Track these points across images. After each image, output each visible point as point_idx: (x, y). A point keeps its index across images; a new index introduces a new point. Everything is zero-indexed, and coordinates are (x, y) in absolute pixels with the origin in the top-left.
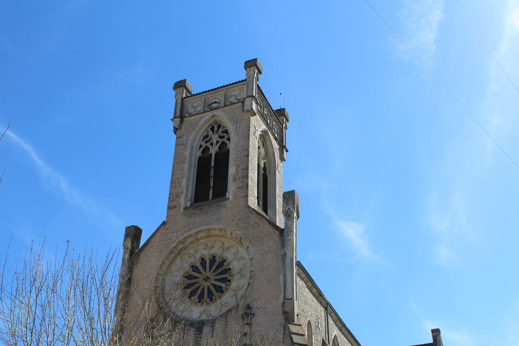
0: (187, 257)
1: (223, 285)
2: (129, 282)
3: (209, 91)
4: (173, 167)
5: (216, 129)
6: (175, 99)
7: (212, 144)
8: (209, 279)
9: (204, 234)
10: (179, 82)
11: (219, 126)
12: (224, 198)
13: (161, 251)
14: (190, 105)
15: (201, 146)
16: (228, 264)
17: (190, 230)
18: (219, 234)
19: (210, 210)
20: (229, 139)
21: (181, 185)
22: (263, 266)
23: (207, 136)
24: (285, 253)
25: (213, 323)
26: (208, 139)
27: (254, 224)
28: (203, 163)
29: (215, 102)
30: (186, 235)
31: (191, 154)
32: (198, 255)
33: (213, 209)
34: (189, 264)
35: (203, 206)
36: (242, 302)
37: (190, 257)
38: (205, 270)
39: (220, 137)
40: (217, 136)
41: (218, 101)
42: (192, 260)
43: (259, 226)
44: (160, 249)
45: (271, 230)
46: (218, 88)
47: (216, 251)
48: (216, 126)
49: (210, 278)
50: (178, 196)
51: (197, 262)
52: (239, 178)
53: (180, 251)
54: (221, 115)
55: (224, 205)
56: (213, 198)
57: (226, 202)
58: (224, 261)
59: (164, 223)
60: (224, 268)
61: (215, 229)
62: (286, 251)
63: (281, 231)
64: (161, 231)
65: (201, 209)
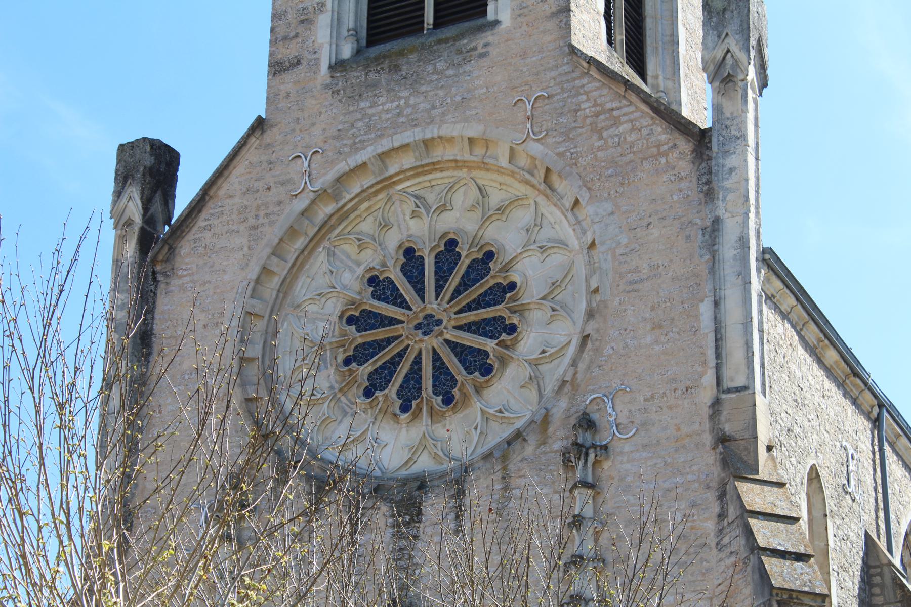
0: (350, 249)
1: (489, 345)
2: (145, 341)
8: (436, 321)
9: (408, 161)
12: (480, 21)
13: (254, 228)
17: (355, 148)
18: (467, 157)
19: (430, 68)
22: (637, 270)
24: (717, 221)
25: (457, 482)
27: (597, 115)
30: (342, 167)
32: (393, 240)
33: (440, 65)
34: (360, 271)
35: (401, 53)
36: (563, 403)
37: (361, 248)
42: (370, 258)
43: (616, 122)
44: (252, 221)
45: (663, 137)
47: (459, 220)
49: (439, 322)
51: (390, 263)
53: (326, 227)
55: (480, 50)
58: (490, 255)
59: (259, 125)
60: (489, 282)
61: (450, 140)
62: (721, 212)
63: (701, 139)
64: (251, 155)
65: (396, 68)
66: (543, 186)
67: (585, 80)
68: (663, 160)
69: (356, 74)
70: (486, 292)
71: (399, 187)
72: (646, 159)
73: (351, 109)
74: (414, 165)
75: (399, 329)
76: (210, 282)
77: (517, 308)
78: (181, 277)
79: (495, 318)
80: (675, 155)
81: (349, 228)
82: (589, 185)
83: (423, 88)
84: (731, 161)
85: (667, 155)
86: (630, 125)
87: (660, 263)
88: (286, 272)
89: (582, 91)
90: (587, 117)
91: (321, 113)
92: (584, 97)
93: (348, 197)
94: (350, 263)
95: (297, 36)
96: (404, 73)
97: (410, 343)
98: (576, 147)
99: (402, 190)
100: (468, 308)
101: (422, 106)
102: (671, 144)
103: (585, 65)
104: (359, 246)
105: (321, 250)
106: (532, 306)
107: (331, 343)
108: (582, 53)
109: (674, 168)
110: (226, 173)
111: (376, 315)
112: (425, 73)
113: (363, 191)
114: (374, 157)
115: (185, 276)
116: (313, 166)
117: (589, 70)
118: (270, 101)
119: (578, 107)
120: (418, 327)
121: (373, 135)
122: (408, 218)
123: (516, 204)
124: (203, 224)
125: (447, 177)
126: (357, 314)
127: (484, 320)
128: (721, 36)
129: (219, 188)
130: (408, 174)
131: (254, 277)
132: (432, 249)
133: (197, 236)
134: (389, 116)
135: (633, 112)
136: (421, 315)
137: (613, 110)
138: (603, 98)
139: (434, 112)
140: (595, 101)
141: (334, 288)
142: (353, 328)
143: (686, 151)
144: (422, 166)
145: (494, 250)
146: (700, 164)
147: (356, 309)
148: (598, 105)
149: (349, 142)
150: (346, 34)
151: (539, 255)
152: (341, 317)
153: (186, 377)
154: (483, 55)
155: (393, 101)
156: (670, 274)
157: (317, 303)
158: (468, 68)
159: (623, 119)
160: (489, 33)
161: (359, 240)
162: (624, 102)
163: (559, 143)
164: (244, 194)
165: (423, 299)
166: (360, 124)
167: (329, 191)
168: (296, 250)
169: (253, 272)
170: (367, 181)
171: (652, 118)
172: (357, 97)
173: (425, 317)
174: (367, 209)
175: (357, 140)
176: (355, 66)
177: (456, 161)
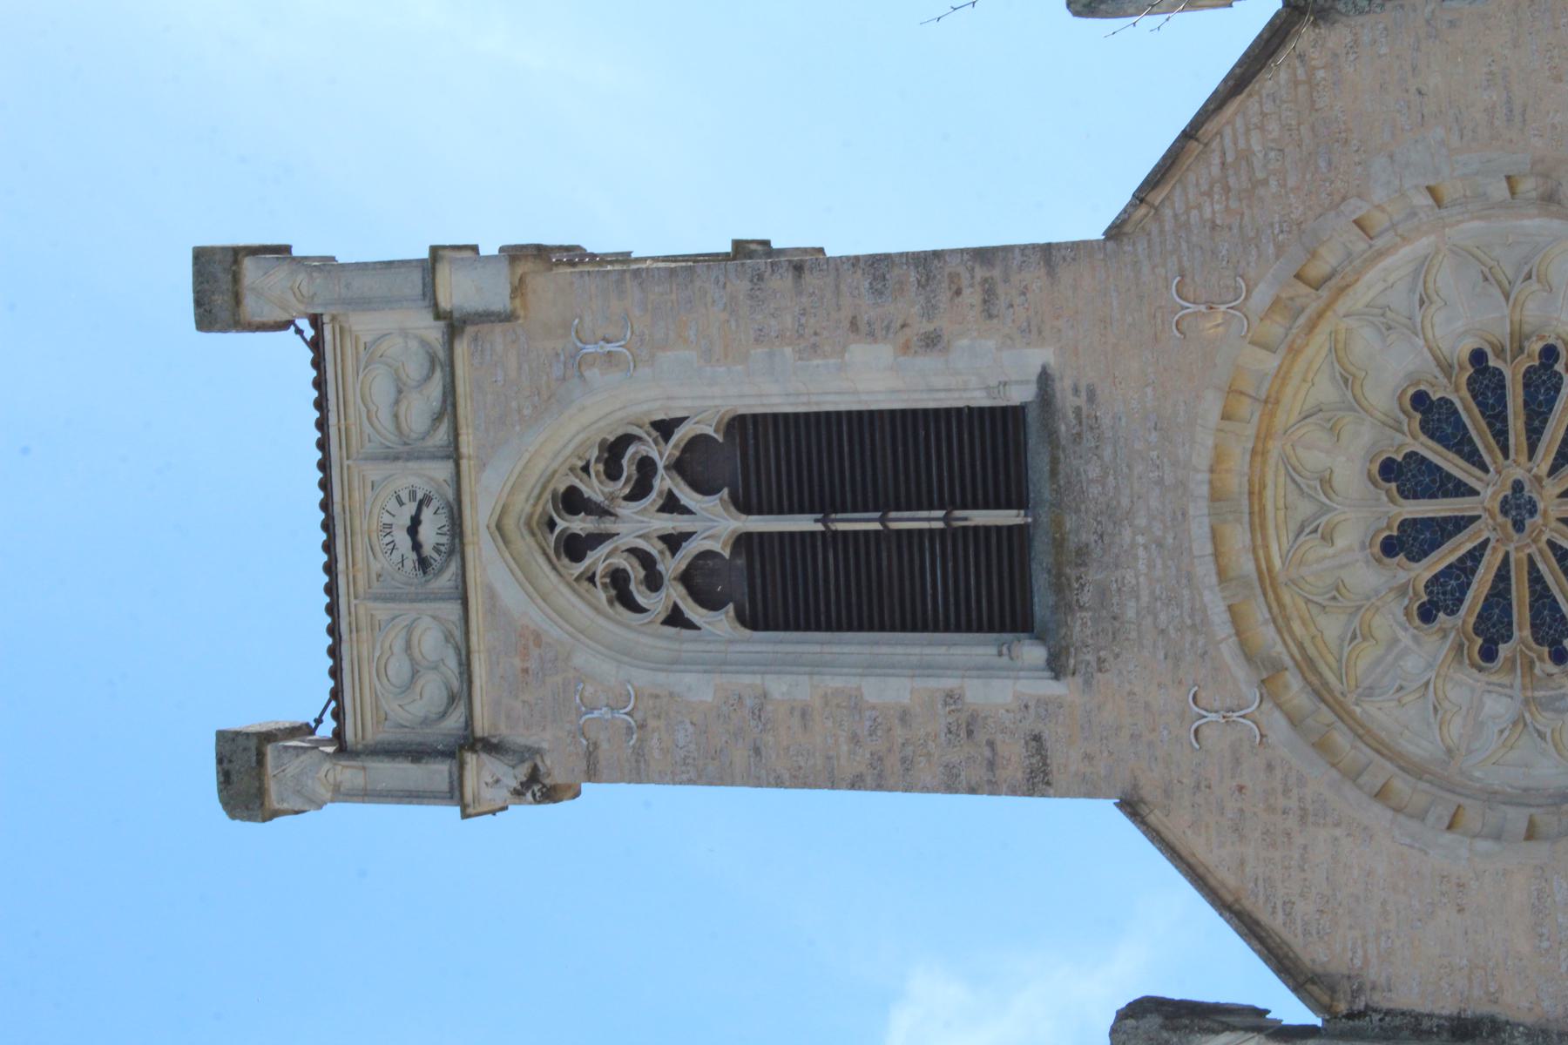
0: (1367, 655)
3: (330, 568)
4: (779, 783)
5: (580, 525)
6: (332, 809)
7: (673, 542)
9: (1238, 538)
10: (226, 779)
11: (572, 501)
12: (1032, 416)
13: (1303, 819)
14: (392, 706)
15: (676, 618)
16: (1446, 368)
18: (1251, 431)
19: (1095, 490)
20: (665, 428)
21: (905, 716)
23: (618, 580)
26: (636, 572)
27: (1227, 189)
28: (781, 593)
29: (413, 529)
30: (1228, 652)
31: (718, 666)
33: (1094, 471)
34: (1406, 639)
35: (1059, 544)
37: (1368, 636)
38: (1460, 524)
40: (627, 510)
41: (411, 508)
42: (1391, 621)
43: (1245, 156)
44: (1292, 823)
45: (1283, 76)
46: (326, 505)
47: (1348, 462)
48: (566, 526)
49: (1518, 486)
50: (970, 726)
51: (1403, 577)
52: (929, 311)
53: (1321, 693)
54: (507, 477)
55: (1082, 401)
56: (1021, 503)
57: (1067, 400)
58: (1420, 400)
59: (1132, 807)
60: (1461, 399)
64: (1176, 825)
65: (1082, 552)
66: (1325, 293)
67: (1168, 212)
68: (1321, 74)
69: (1078, 628)
70: (1479, 404)
71: (1277, 563)
72: (1313, 102)
73: (1133, 635)
74: (1247, 526)
75: (1543, 465)
76: (1384, 903)
77: (1516, 345)
78: (1366, 961)
79: (1526, 386)
80: (1315, 55)
81: (1331, 659)
82: (1337, 198)
83: (1125, 502)
85: (1315, 68)
86: (1253, 133)
87: (1485, 70)
88: (1388, 765)
89: (1183, 218)
90: (1227, 207)
91: (1131, 693)
92: (1194, 213)
93: (1279, 648)
94: (1390, 658)
95: (991, 744)
96: (1095, 537)
97: (1544, 538)
98: (1272, 225)
99: (1283, 558)
100: (1501, 436)
101: (1154, 503)
102: (1297, 63)
103: (1143, 210)
104: (1364, 639)
105: (1358, 710)
106: (1517, 318)
107: (1524, 688)
108: (1125, 211)
109: (1336, 55)
110: (1201, 870)
111: (1487, 605)
112: (1101, 499)
113: (1274, 621)
114: (1222, 590)
115: (1365, 952)
116: (1217, 705)
117: (1152, 206)
118: (1092, 793)
119: (1209, 224)
120: (1519, 526)
121: (1186, 592)
122: (1330, 551)
123: (1341, 354)
124: (1280, 916)
125: (1276, 476)
126: (1480, 641)
127: (1526, 404)
129: (1223, 885)
130: (1259, 542)
131: (1389, 814)
132: (1392, 500)
133: (1299, 931)
134: (1159, 562)
135: (1234, 130)
136: (1500, 519)
137: (1223, 164)
138: (1202, 181)
139: (1169, 479)
140: (1203, 194)
141: (1427, 684)
142: (1502, 647)
143: (1313, 36)
144: (1251, 513)
145: (1411, 392)
146: (1339, 12)
147: (1471, 641)
148: (1211, 188)
149: (1189, 637)
150: (1005, 659)
151: (1434, 307)
152: (1480, 670)
153: (1545, 944)
154: (1092, 396)
155: (1136, 558)
156: (1506, 52)
157: (1448, 717)
158: (1106, 422)
159: (1242, 144)
160: (1058, 385)
161: (1354, 637)
162: (1214, 145)
163: (1259, 256)
164: (1242, 838)
165: (1473, 519)
166: (1163, 617)
167: (1265, 676)
168: (1353, 747)
169: (1378, 815)
170: (1258, 613)
171: (1250, 95)
172: (1117, 624)
173: (1504, 512)
174: (1304, 623)
175: (1189, 622)
176: (1063, 631)
177: (1254, 452)
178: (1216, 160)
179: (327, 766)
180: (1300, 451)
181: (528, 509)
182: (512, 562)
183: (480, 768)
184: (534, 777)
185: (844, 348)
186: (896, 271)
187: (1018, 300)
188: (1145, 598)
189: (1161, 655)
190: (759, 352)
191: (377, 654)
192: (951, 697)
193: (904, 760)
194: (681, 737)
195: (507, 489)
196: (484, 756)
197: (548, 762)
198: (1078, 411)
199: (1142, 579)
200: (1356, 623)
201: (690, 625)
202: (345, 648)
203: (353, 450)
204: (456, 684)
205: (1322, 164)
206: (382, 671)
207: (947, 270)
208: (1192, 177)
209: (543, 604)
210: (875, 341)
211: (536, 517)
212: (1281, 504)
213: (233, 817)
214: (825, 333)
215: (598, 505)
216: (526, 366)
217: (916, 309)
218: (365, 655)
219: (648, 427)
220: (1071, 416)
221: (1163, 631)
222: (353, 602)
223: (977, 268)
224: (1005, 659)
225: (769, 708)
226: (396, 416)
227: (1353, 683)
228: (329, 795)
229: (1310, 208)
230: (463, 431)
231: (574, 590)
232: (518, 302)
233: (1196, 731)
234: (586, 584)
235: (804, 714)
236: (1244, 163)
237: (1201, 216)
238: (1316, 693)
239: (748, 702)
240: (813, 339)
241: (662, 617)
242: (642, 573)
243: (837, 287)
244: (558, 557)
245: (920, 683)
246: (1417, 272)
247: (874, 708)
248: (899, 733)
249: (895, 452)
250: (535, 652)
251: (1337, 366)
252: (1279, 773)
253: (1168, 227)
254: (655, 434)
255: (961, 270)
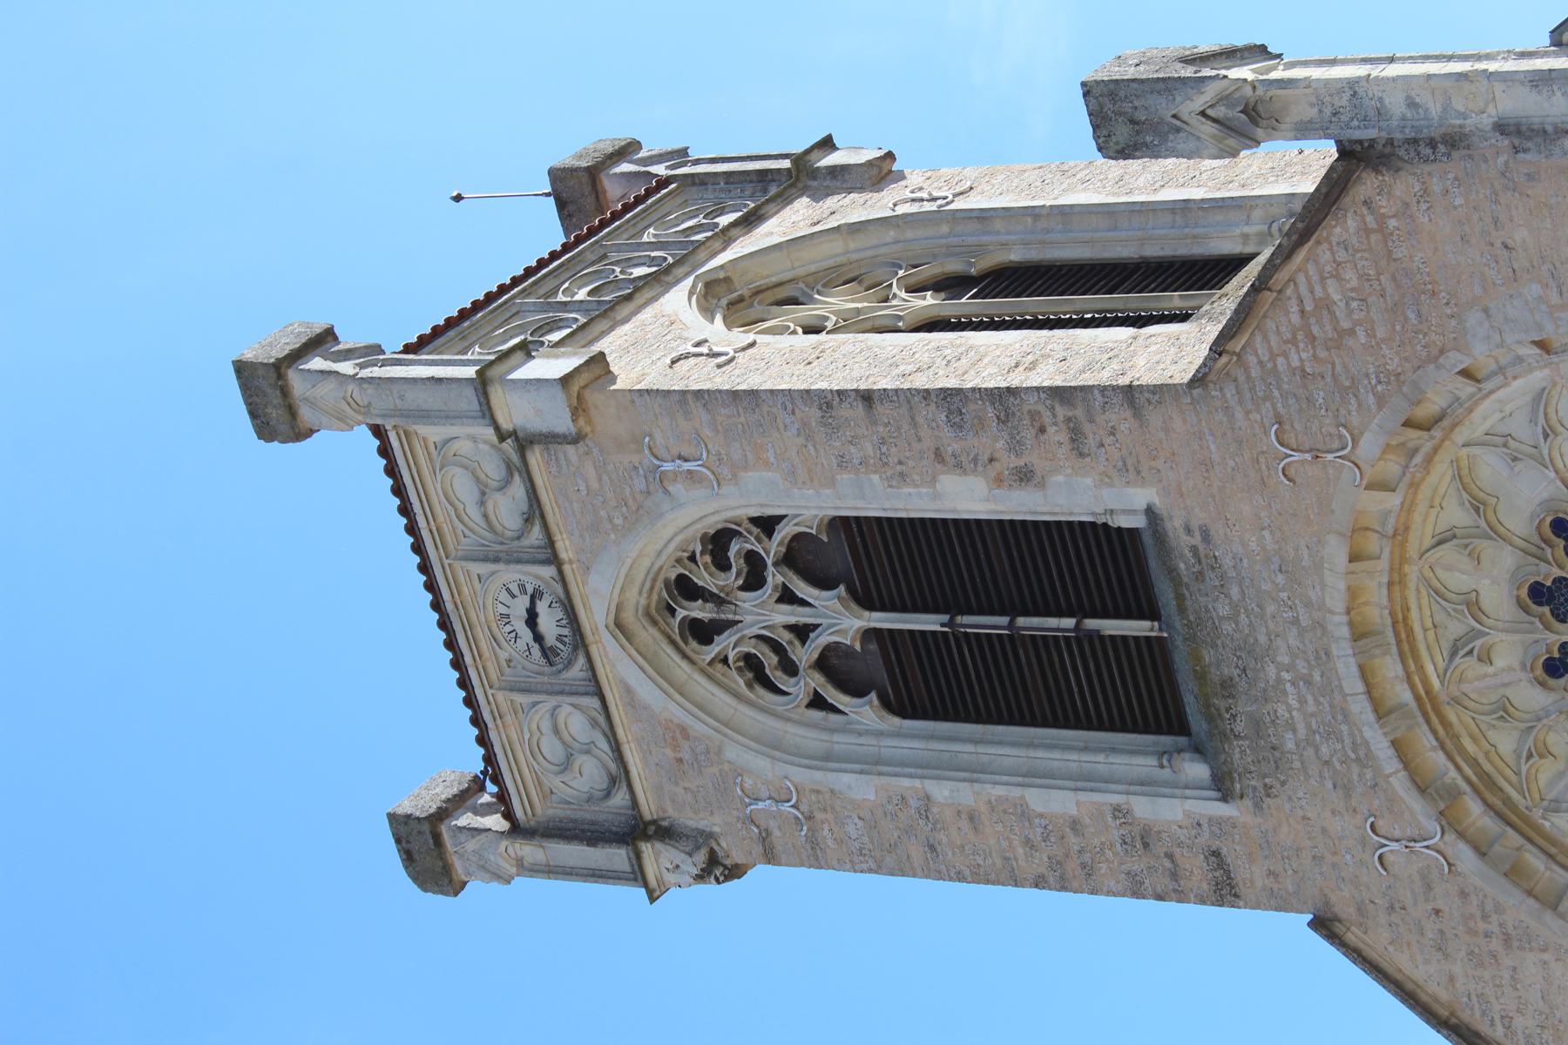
3: (457, 664)
5: (700, 611)
7: (802, 632)
9: (1389, 668)
10: (408, 858)
11: (686, 588)
12: (1147, 540)
13: (1507, 940)
15: (818, 702)
17: (1365, 759)
18: (1383, 564)
19: (1228, 627)
20: (767, 525)
21: (1075, 825)
23: (751, 663)
24: (1501, 128)
26: (770, 660)
28: (922, 685)
29: (532, 619)
30: (1399, 783)
31: (872, 764)
33: (1223, 610)
35: (1201, 677)
37: (1545, 752)
39: (754, 581)
40: (747, 600)
41: (524, 602)
43: (1325, 305)
44: (1496, 944)
45: (1351, 223)
46: (437, 605)
47: (1495, 582)
48: (687, 608)
50: (1145, 839)
52: (1015, 446)
53: (1507, 814)
54: (613, 577)
55: (1197, 540)
56: (1152, 614)
59: (1324, 925)
61: (1353, 593)
62: (1486, 121)
63: (1355, 157)
64: (1377, 942)
65: (1227, 686)
66: (1437, 433)
67: (1251, 359)
69: (1237, 756)
72: (1390, 252)
73: (1297, 765)
80: (1384, 203)
81: (1508, 772)
82: (1435, 352)
83: (1262, 639)
84: (1396, 104)
85: (1384, 216)
86: (1329, 282)
89: (1270, 365)
92: (1280, 360)
93: (1453, 773)
95: (1170, 856)
101: (1293, 642)
102: (1365, 210)
103: (1224, 359)
104: (1541, 756)
105: (1547, 824)
108: (1204, 364)
110: (1410, 986)
112: (1236, 636)
113: (1443, 747)
116: (1397, 834)
118: (1283, 906)
121: (1344, 728)
122: (1491, 670)
123: (1467, 480)
128: (1177, 126)
129: (1437, 1000)
130: (1412, 667)
132: (1548, 627)
134: (1310, 699)
138: (1283, 329)
144: (1399, 643)
145: (1549, 519)
146: (1400, 158)
148: (1294, 336)
149: (1355, 769)
150: (1167, 770)
154: (1206, 536)
158: (1227, 562)
160: (1168, 525)
162: (1289, 292)
163: (1360, 405)
164: (1446, 956)
166: (1324, 750)
167: (1442, 806)
171: (1318, 243)
172: (1277, 754)
174: (1475, 740)
175: (1353, 756)
176: (1223, 757)
177: (1390, 584)
178: (1295, 309)
179: (504, 843)
180: (1439, 572)
181: (643, 601)
182: (640, 659)
183: (657, 856)
184: (713, 860)
185: (933, 481)
186: (972, 406)
187: (1108, 440)
188: (1302, 732)
189: (1329, 785)
190: (844, 478)
191: (527, 736)
192: (1117, 810)
193: (1083, 866)
194: (851, 829)
195: (617, 591)
196: (658, 845)
197: (724, 844)
198: (1194, 549)
199: (1294, 713)
200: (1530, 742)
201: (834, 709)
202: (493, 735)
203: (451, 547)
204: (613, 767)
205: (1412, 316)
206: (535, 751)
207: (1026, 408)
208: (1271, 325)
209: (681, 700)
210: (965, 473)
211: (653, 605)
212: (1429, 624)
213: (426, 890)
214: (911, 463)
215: (712, 594)
216: (605, 478)
217: (1000, 444)
218: (514, 736)
219: (746, 524)
220: (1189, 555)
221: (1326, 762)
222: (490, 692)
223: (1058, 408)
224: (1167, 770)
225: (935, 810)
226: (485, 516)
227: (1537, 796)
228: (514, 870)
229: (1406, 359)
230: (557, 537)
231: (710, 677)
232: (581, 422)
233: (1380, 857)
234: (720, 666)
235: (971, 819)
236: (1325, 312)
237: (1289, 364)
238: (1499, 815)
239: (913, 803)
240: (899, 468)
241: (806, 701)
242: (775, 659)
243: (912, 418)
244: (686, 643)
245: (1082, 796)
246: (1535, 411)
247: (1041, 816)
248: (1074, 841)
249: (1010, 556)
250: (685, 745)
251: (1465, 495)
252: (1474, 901)
253: (1255, 372)
254: (756, 530)
255: (1041, 408)
